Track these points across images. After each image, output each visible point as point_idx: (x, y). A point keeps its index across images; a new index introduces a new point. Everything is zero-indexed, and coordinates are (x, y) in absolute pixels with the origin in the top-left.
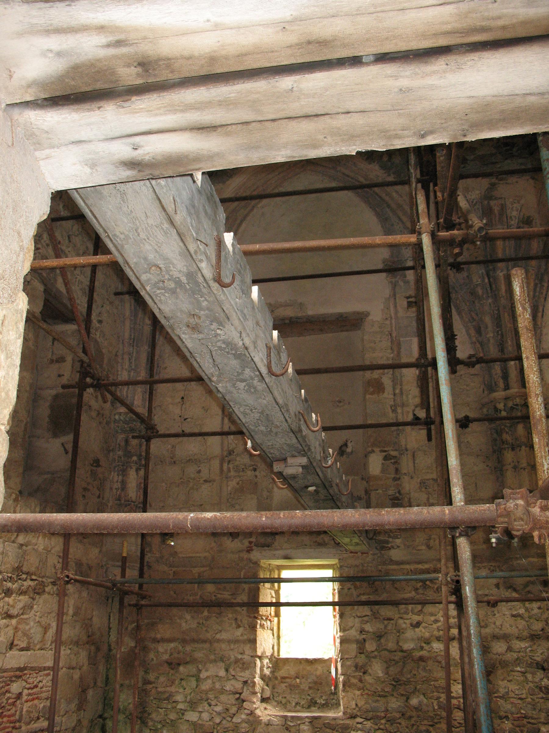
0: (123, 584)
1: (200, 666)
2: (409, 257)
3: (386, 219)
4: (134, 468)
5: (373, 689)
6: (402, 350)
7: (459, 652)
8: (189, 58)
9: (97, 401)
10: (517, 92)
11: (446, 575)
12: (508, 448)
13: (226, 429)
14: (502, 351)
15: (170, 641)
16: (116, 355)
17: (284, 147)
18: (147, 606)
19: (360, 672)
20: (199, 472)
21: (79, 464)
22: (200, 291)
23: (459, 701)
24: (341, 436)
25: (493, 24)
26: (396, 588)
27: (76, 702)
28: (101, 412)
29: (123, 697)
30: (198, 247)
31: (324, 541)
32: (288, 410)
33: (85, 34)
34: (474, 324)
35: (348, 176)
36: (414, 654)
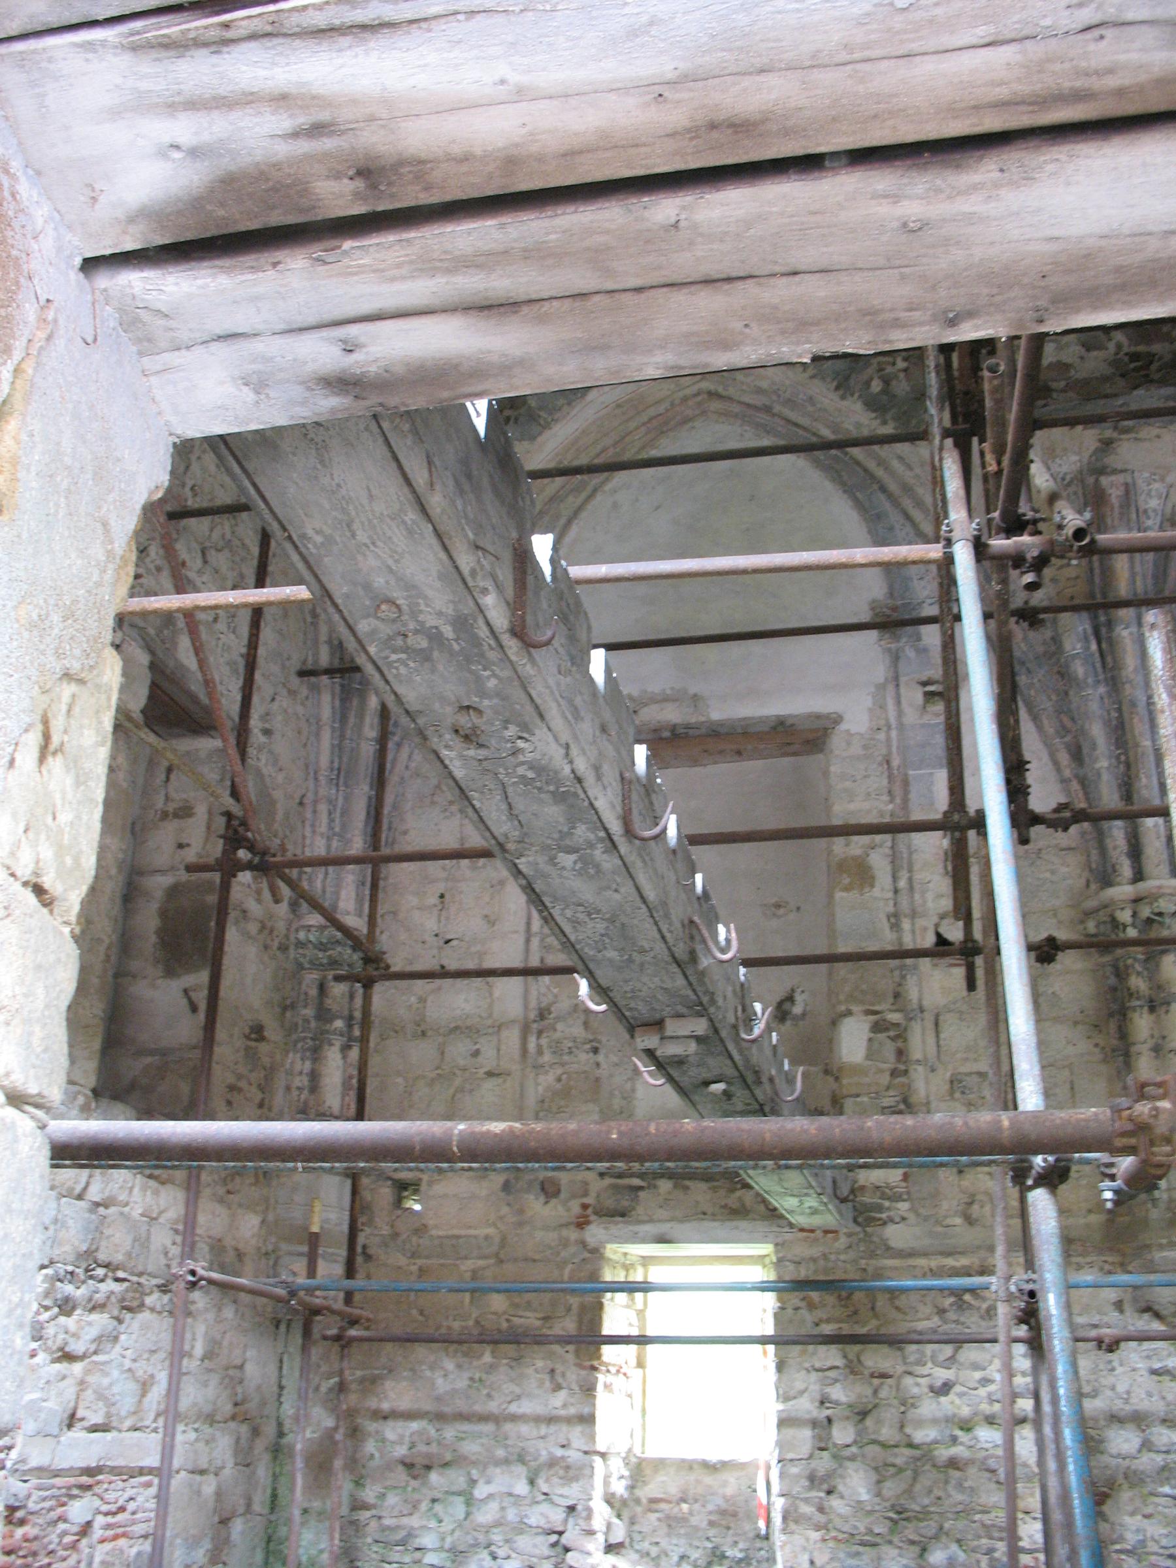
0: (310, 1291)
1: (474, 1472)
2: (928, 597)
3: (879, 517)
4: (338, 1044)
5: (846, 1528)
6: (913, 796)
7: (1035, 1449)
8: (466, 158)
9: (259, 901)
10: (1150, 228)
11: (1008, 1278)
12: (1141, 1007)
13: (534, 962)
14: (1128, 797)
15: (409, 1416)
16: (301, 804)
17: (661, 347)
18: (361, 1340)
19: (820, 1490)
20: (476, 1053)
21: (221, 1034)
22: (482, 655)
23: (1036, 1559)
24: (779, 980)
25: (1096, 84)
26: (898, 1308)
27: (207, 1545)
28: (269, 924)
29: (307, 1536)
30: (479, 561)
31: (743, 1205)
32: (667, 916)
33: (249, 111)
34: (1068, 739)
35: (796, 425)
36: (936, 1453)
